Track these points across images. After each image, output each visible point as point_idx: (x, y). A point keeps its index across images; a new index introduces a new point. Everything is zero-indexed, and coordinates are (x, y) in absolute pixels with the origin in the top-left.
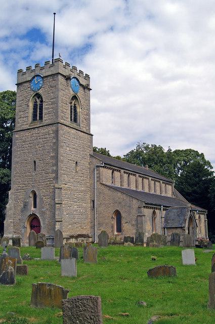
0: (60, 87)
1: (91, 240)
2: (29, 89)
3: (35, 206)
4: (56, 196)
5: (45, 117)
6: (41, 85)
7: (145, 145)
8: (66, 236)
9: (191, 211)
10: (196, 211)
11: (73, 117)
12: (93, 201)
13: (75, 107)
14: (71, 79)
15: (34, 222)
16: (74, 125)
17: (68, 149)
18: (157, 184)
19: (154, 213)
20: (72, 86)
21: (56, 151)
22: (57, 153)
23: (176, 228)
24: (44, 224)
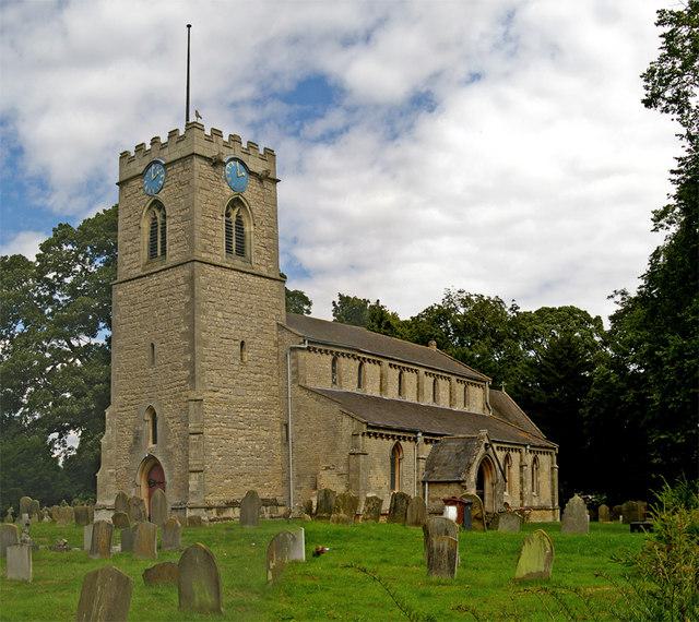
0: (197, 182)
1: (282, 510)
2: (142, 191)
3: (155, 442)
4: (191, 416)
5: (170, 250)
6: (161, 182)
7: (463, 296)
8: (217, 504)
9: (486, 444)
10: (525, 446)
11: (159, 240)
12: (287, 426)
13: (239, 222)
14: (225, 164)
15: (154, 473)
16: (238, 262)
17: (220, 314)
18: (442, 383)
19: (397, 449)
20: (229, 179)
21: (191, 320)
22: (192, 326)
23: (449, 483)
24: (171, 477)
